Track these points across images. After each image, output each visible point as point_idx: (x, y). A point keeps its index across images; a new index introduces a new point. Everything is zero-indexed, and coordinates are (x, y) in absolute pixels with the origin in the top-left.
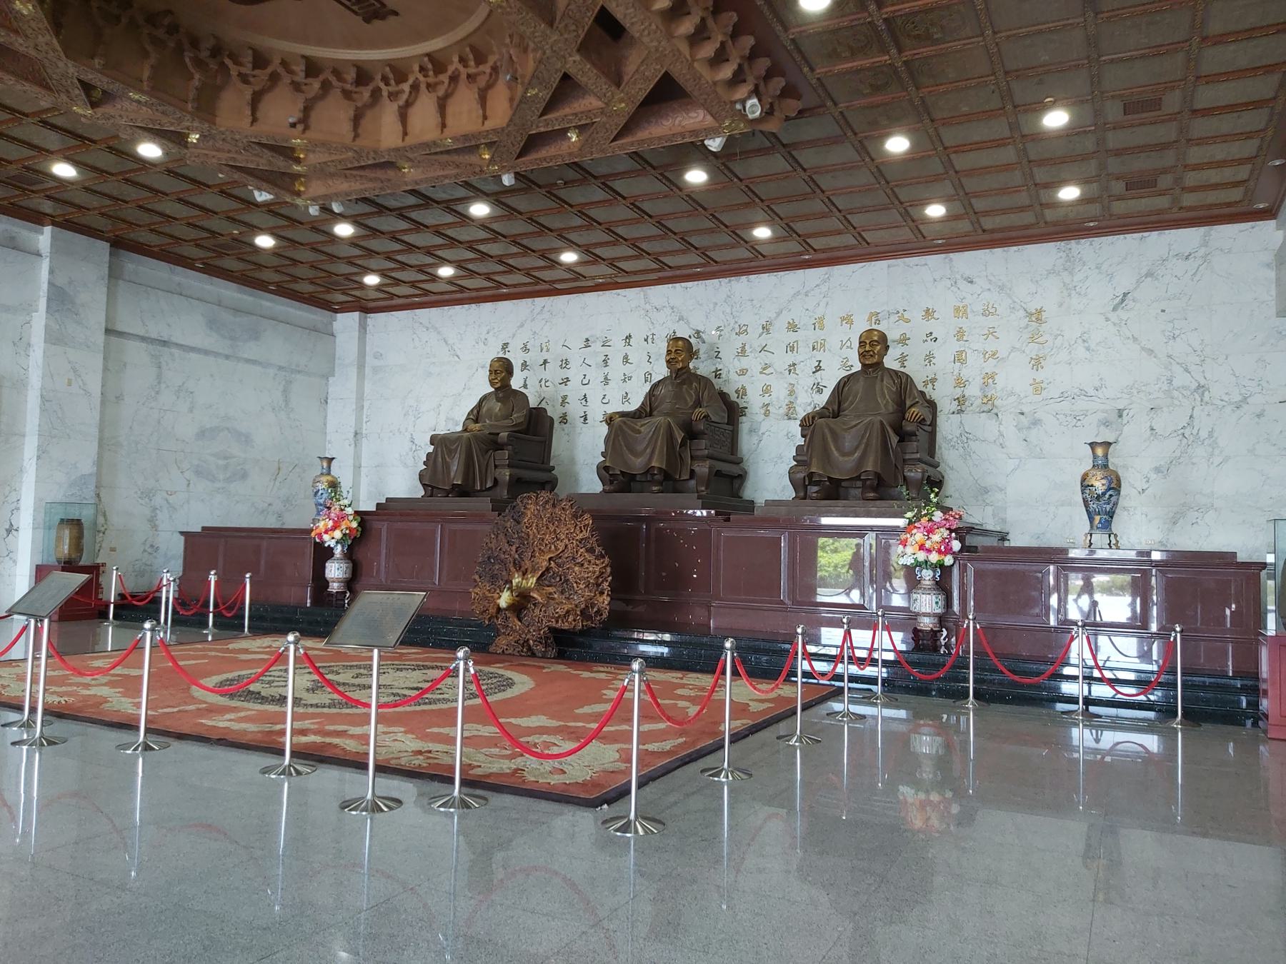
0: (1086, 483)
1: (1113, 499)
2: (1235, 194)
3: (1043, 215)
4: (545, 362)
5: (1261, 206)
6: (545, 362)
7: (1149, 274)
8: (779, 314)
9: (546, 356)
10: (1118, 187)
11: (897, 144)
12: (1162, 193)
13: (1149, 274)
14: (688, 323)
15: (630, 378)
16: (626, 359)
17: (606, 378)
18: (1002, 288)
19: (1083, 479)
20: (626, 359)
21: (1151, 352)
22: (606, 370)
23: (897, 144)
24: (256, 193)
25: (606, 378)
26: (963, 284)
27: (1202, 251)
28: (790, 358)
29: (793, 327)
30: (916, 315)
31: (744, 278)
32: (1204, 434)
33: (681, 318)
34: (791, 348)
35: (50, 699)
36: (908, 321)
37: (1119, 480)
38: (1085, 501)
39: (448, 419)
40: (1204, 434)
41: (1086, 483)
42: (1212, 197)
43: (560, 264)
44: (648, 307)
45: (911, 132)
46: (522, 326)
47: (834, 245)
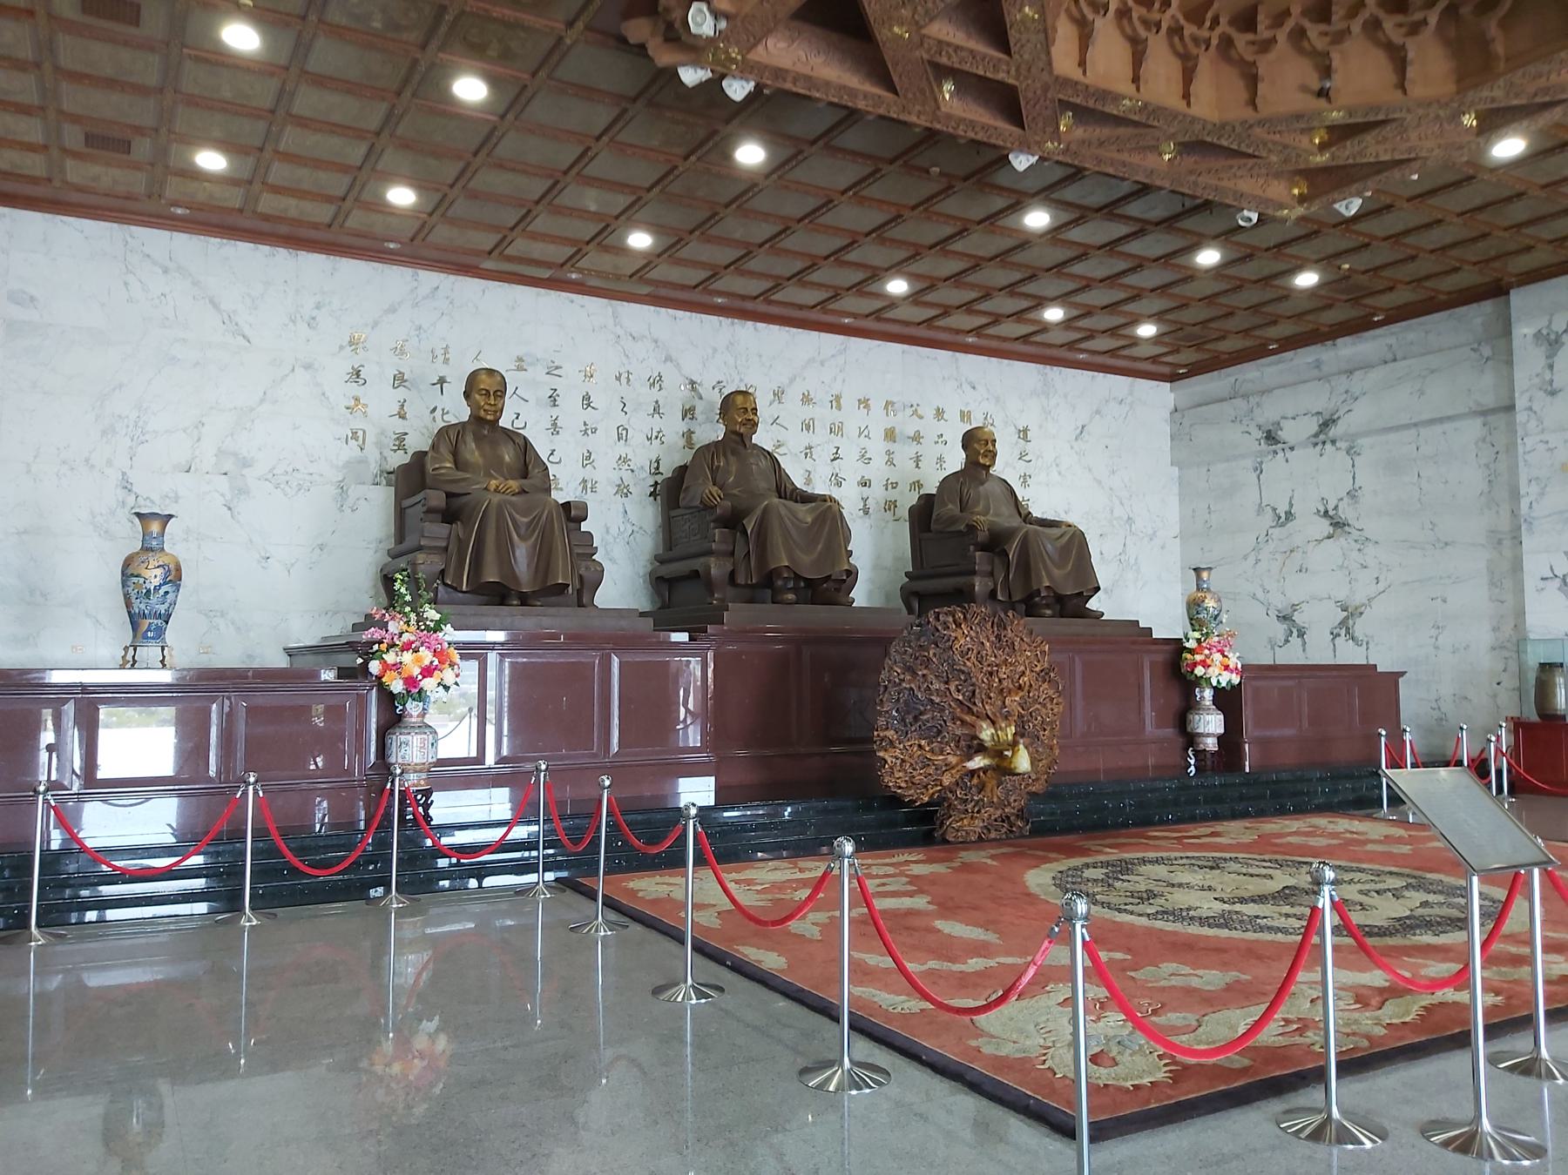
0: (129, 571)
1: (170, 597)
2: (323, 213)
3: (257, 200)
4: (442, 381)
5: (574, 276)
6: (442, 381)
7: (1098, 412)
8: (792, 380)
9: (444, 371)
10: (73, 136)
11: (470, 89)
12: (137, 167)
13: (1098, 412)
14: (678, 366)
15: (594, 431)
16: (587, 401)
17: (555, 425)
18: (997, 400)
19: (128, 563)
20: (587, 401)
21: (1099, 482)
22: (555, 412)
23: (470, 89)
24: (1340, 207)
25: (555, 425)
26: (966, 387)
27: (1130, 399)
28: (806, 439)
29: (806, 399)
30: (929, 413)
31: (750, 323)
32: (1132, 561)
33: (668, 359)
34: (808, 426)
35: (680, 880)
36: (921, 417)
37: (178, 569)
38: (127, 597)
39: (221, 453)
40: (1132, 561)
41: (129, 571)
42: (291, 206)
43: (1142, 339)
44: (619, 331)
45: (493, 80)
46: (392, 310)
47: (536, 255)
